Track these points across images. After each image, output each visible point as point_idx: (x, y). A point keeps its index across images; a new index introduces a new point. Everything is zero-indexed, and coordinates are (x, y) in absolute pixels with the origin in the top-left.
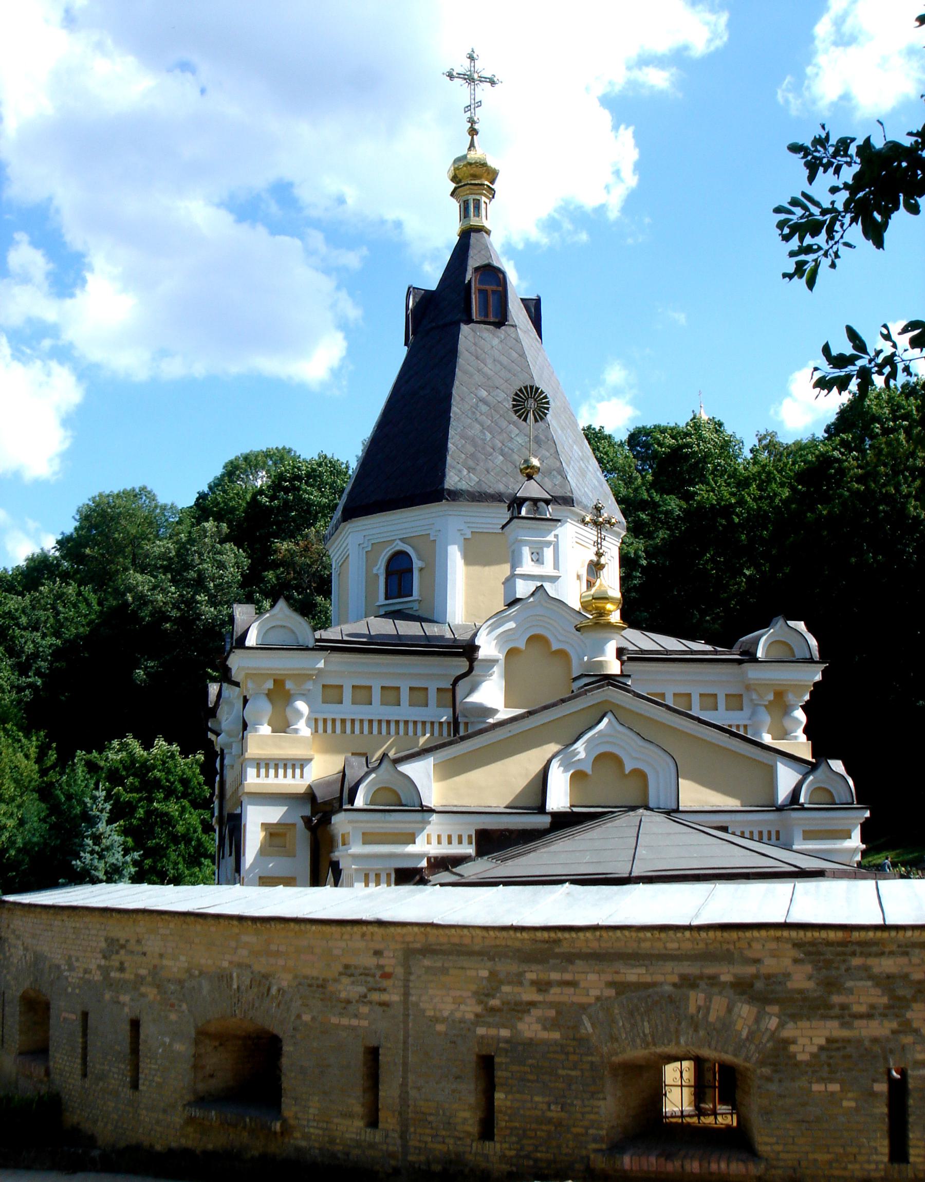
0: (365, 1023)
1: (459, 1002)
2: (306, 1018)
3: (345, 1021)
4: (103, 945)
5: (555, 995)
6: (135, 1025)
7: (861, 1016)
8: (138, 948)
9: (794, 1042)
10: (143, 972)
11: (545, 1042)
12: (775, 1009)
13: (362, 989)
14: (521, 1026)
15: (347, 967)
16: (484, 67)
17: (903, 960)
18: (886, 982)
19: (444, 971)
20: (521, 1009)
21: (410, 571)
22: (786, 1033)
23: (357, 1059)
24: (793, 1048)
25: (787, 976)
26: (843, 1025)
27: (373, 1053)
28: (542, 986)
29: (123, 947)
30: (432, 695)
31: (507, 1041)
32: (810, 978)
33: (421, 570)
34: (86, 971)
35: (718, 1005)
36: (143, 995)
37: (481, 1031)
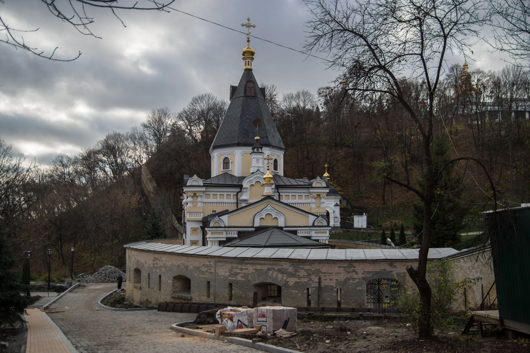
0: (207, 276)
1: (225, 272)
2: (196, 275)
3: (203, 276)
4: (153, 258)
5: (244, 271)
6: (160, 276)
7: (302, 277)
8: (161, 260)
9: (289, 282)
10: (162, 265)
11: (241, 281)
12: (285, 275)
13: (207, 269)
14: (237, 277)
15: (204, 264)
16: (252, 22)
17: (310, 266)
18: (307, 270)
19: (222, 266)
20: (237, 274)
21: (229, 163)
22: (287, 280)
23: (205, 284)
24: (289, 283)
25: (288, 269)
26: (299, 279)
27: (209, 282)
28: (241, 269)
29: (157, 259)
30: (232, 196)
31: (235, 280)
32: (292, 269)
33: (232, 162)
34: (149, 264)
35: (275, 274)
36: (162, 270)
37: (230, 278)
